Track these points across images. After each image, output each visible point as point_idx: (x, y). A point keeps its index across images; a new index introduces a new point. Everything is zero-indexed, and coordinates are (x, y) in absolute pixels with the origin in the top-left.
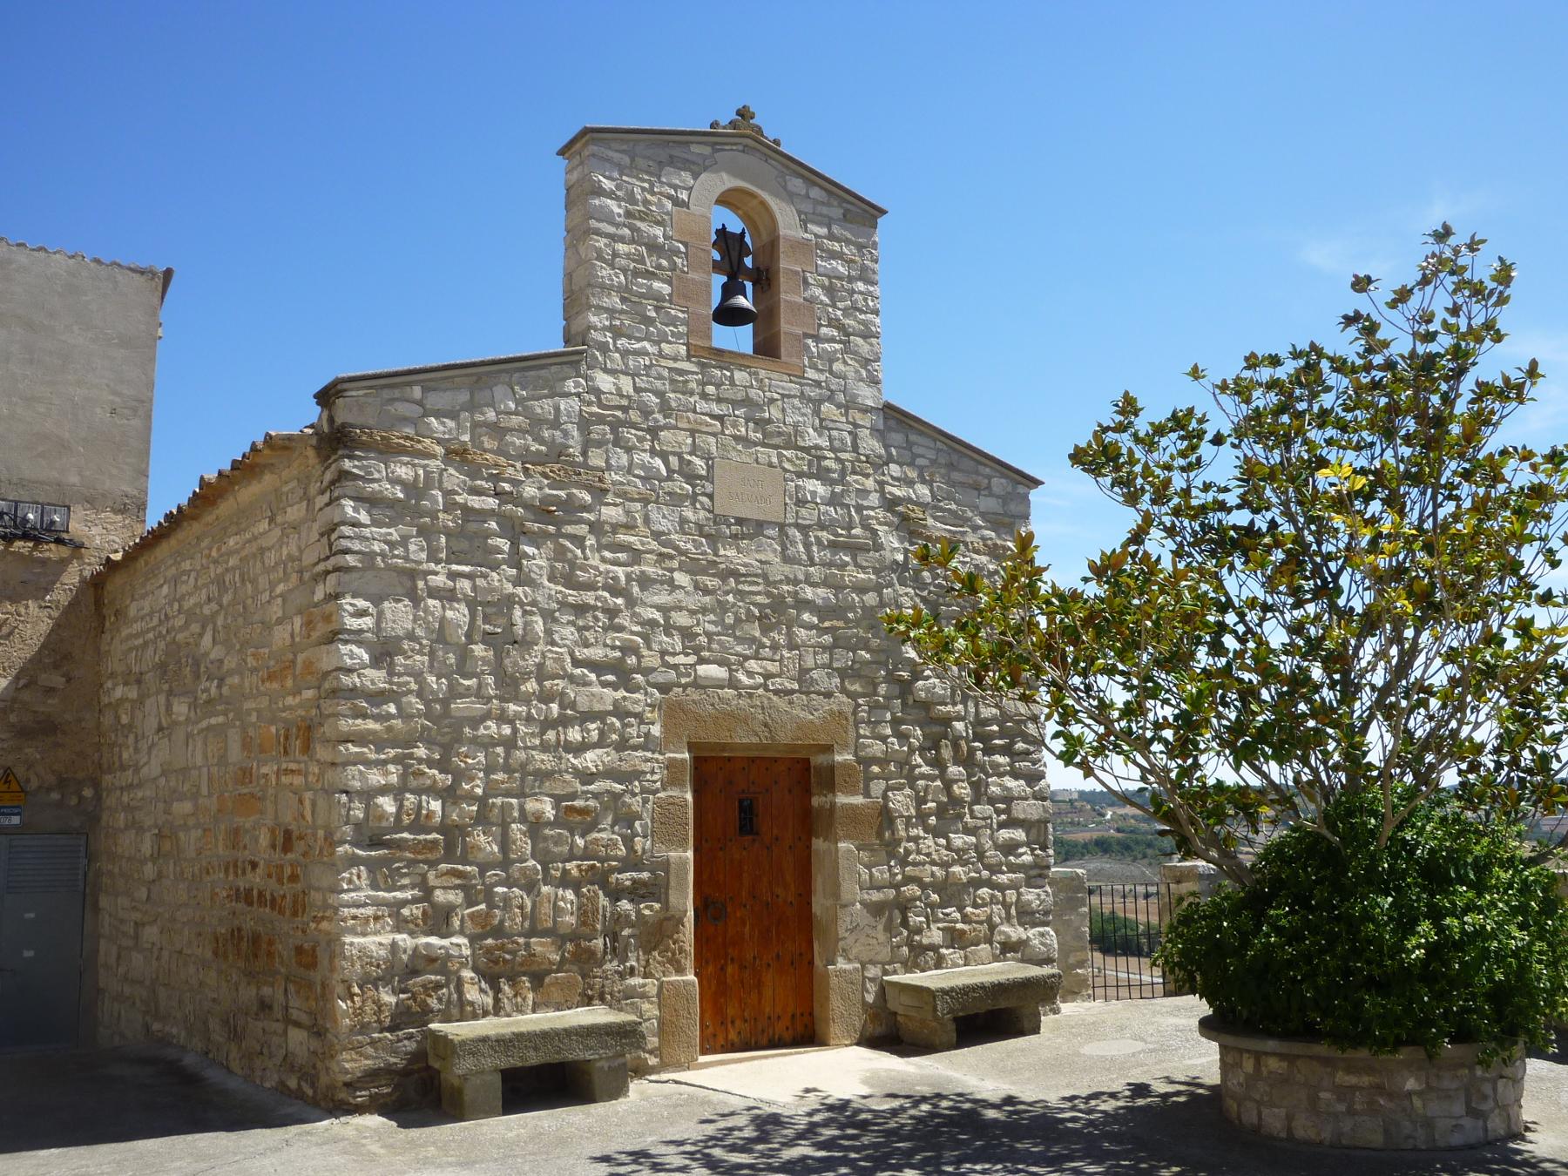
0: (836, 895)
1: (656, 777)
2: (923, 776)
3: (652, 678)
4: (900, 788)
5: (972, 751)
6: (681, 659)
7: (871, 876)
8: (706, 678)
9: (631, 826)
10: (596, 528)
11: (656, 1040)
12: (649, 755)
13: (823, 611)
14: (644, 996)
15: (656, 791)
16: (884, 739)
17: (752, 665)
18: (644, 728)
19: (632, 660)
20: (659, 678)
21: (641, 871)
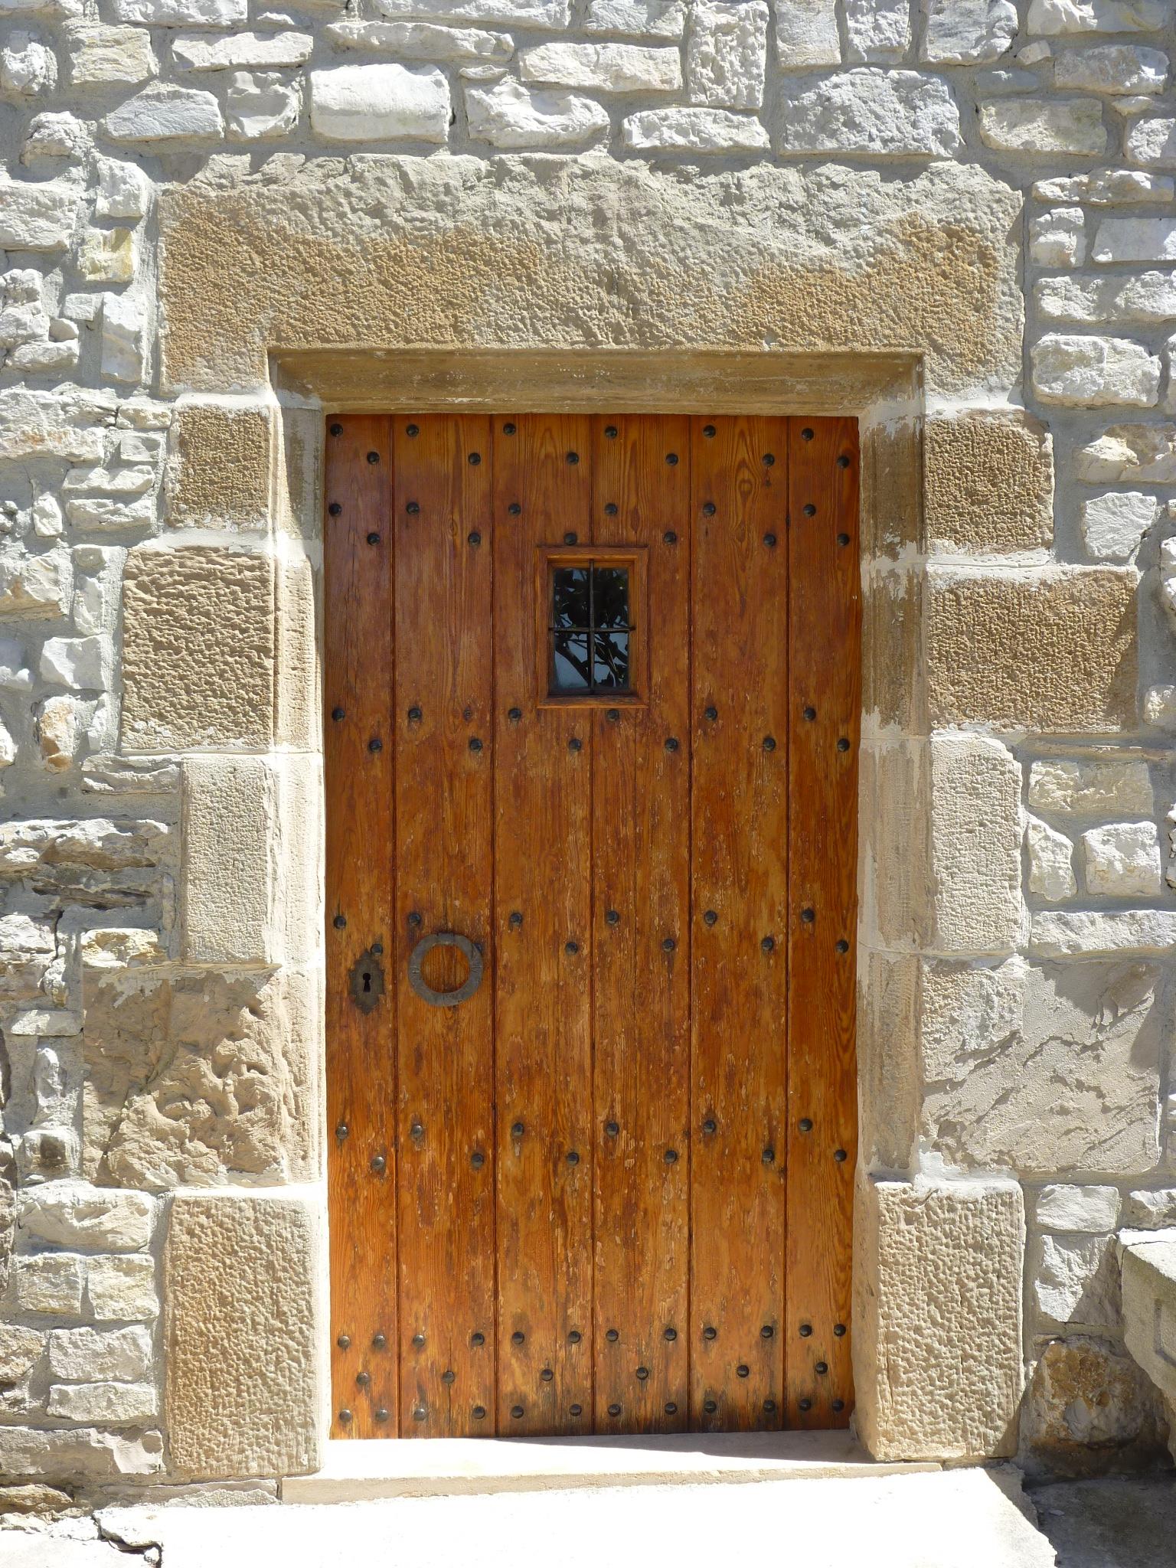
0: (921, 924)
1: (127, 480)
3: (118, 122)
6: (245, 48)
7: (1081, 859)
8: (348, 113)
9: (30, 658)
12: (101, 398)
14: (95, 1245)
15: (137, 532)
17: (561, 61)
18: (81, 305)
20: (150, 120)
21: (77, 814)
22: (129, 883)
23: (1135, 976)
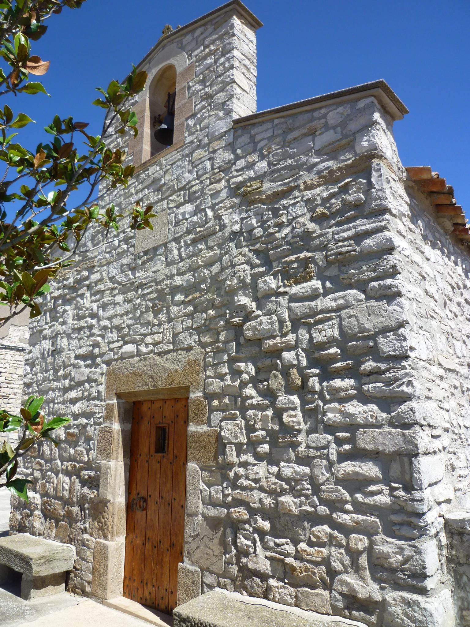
2: (253, 407)
4: (233, 418)
5: (305, 379)
10: (89, 287)
11: (90, 576)
13: (186, 290)
16: (221, 377)
19: (96, 351)
22: (93, 483)
23: (219, 523)
